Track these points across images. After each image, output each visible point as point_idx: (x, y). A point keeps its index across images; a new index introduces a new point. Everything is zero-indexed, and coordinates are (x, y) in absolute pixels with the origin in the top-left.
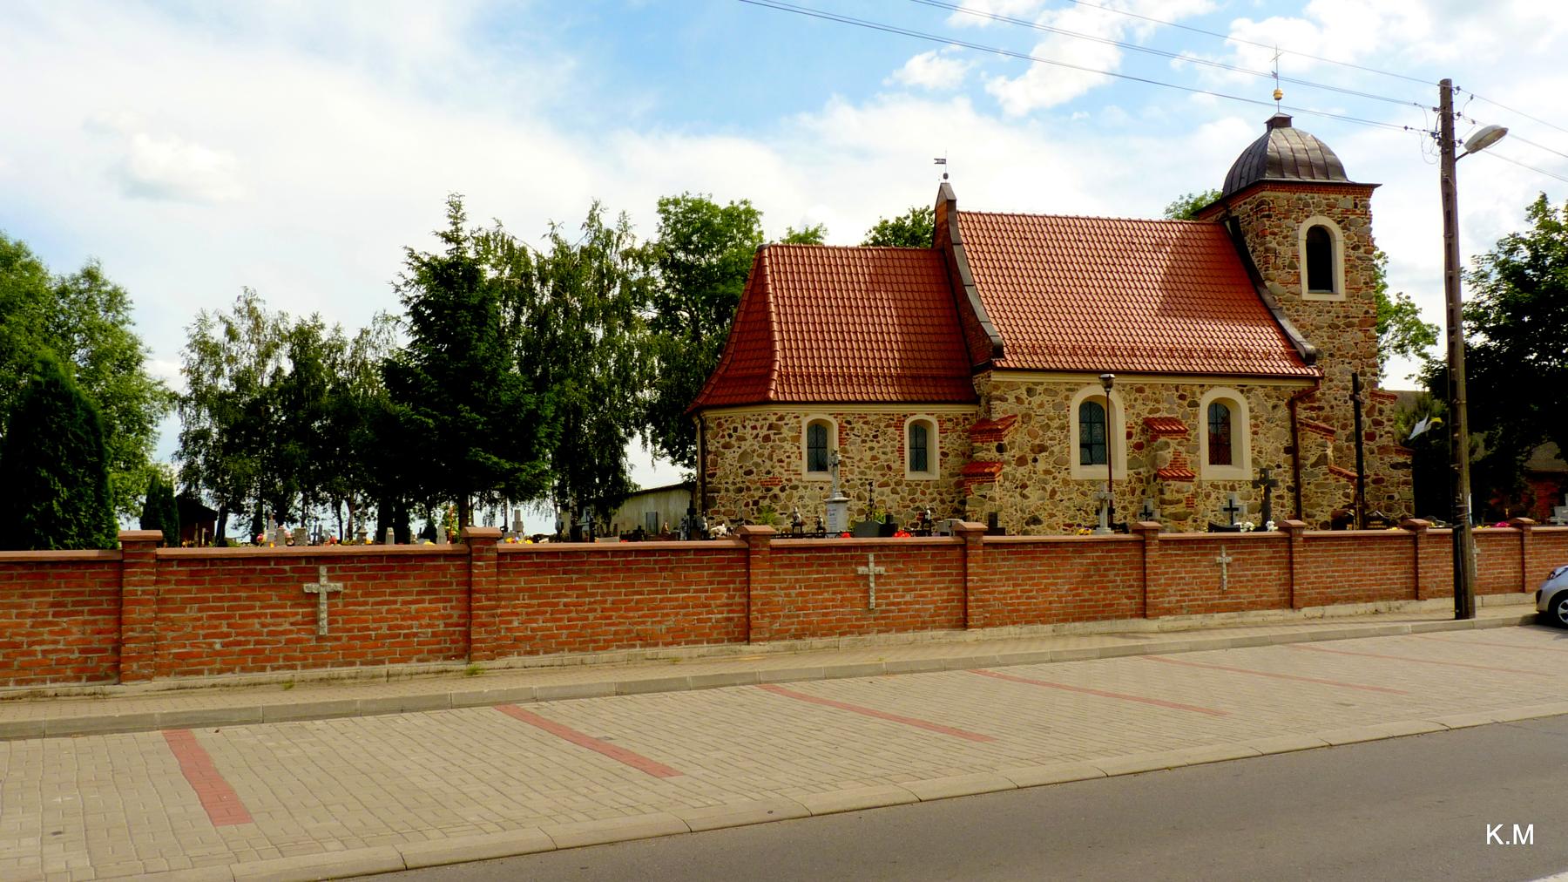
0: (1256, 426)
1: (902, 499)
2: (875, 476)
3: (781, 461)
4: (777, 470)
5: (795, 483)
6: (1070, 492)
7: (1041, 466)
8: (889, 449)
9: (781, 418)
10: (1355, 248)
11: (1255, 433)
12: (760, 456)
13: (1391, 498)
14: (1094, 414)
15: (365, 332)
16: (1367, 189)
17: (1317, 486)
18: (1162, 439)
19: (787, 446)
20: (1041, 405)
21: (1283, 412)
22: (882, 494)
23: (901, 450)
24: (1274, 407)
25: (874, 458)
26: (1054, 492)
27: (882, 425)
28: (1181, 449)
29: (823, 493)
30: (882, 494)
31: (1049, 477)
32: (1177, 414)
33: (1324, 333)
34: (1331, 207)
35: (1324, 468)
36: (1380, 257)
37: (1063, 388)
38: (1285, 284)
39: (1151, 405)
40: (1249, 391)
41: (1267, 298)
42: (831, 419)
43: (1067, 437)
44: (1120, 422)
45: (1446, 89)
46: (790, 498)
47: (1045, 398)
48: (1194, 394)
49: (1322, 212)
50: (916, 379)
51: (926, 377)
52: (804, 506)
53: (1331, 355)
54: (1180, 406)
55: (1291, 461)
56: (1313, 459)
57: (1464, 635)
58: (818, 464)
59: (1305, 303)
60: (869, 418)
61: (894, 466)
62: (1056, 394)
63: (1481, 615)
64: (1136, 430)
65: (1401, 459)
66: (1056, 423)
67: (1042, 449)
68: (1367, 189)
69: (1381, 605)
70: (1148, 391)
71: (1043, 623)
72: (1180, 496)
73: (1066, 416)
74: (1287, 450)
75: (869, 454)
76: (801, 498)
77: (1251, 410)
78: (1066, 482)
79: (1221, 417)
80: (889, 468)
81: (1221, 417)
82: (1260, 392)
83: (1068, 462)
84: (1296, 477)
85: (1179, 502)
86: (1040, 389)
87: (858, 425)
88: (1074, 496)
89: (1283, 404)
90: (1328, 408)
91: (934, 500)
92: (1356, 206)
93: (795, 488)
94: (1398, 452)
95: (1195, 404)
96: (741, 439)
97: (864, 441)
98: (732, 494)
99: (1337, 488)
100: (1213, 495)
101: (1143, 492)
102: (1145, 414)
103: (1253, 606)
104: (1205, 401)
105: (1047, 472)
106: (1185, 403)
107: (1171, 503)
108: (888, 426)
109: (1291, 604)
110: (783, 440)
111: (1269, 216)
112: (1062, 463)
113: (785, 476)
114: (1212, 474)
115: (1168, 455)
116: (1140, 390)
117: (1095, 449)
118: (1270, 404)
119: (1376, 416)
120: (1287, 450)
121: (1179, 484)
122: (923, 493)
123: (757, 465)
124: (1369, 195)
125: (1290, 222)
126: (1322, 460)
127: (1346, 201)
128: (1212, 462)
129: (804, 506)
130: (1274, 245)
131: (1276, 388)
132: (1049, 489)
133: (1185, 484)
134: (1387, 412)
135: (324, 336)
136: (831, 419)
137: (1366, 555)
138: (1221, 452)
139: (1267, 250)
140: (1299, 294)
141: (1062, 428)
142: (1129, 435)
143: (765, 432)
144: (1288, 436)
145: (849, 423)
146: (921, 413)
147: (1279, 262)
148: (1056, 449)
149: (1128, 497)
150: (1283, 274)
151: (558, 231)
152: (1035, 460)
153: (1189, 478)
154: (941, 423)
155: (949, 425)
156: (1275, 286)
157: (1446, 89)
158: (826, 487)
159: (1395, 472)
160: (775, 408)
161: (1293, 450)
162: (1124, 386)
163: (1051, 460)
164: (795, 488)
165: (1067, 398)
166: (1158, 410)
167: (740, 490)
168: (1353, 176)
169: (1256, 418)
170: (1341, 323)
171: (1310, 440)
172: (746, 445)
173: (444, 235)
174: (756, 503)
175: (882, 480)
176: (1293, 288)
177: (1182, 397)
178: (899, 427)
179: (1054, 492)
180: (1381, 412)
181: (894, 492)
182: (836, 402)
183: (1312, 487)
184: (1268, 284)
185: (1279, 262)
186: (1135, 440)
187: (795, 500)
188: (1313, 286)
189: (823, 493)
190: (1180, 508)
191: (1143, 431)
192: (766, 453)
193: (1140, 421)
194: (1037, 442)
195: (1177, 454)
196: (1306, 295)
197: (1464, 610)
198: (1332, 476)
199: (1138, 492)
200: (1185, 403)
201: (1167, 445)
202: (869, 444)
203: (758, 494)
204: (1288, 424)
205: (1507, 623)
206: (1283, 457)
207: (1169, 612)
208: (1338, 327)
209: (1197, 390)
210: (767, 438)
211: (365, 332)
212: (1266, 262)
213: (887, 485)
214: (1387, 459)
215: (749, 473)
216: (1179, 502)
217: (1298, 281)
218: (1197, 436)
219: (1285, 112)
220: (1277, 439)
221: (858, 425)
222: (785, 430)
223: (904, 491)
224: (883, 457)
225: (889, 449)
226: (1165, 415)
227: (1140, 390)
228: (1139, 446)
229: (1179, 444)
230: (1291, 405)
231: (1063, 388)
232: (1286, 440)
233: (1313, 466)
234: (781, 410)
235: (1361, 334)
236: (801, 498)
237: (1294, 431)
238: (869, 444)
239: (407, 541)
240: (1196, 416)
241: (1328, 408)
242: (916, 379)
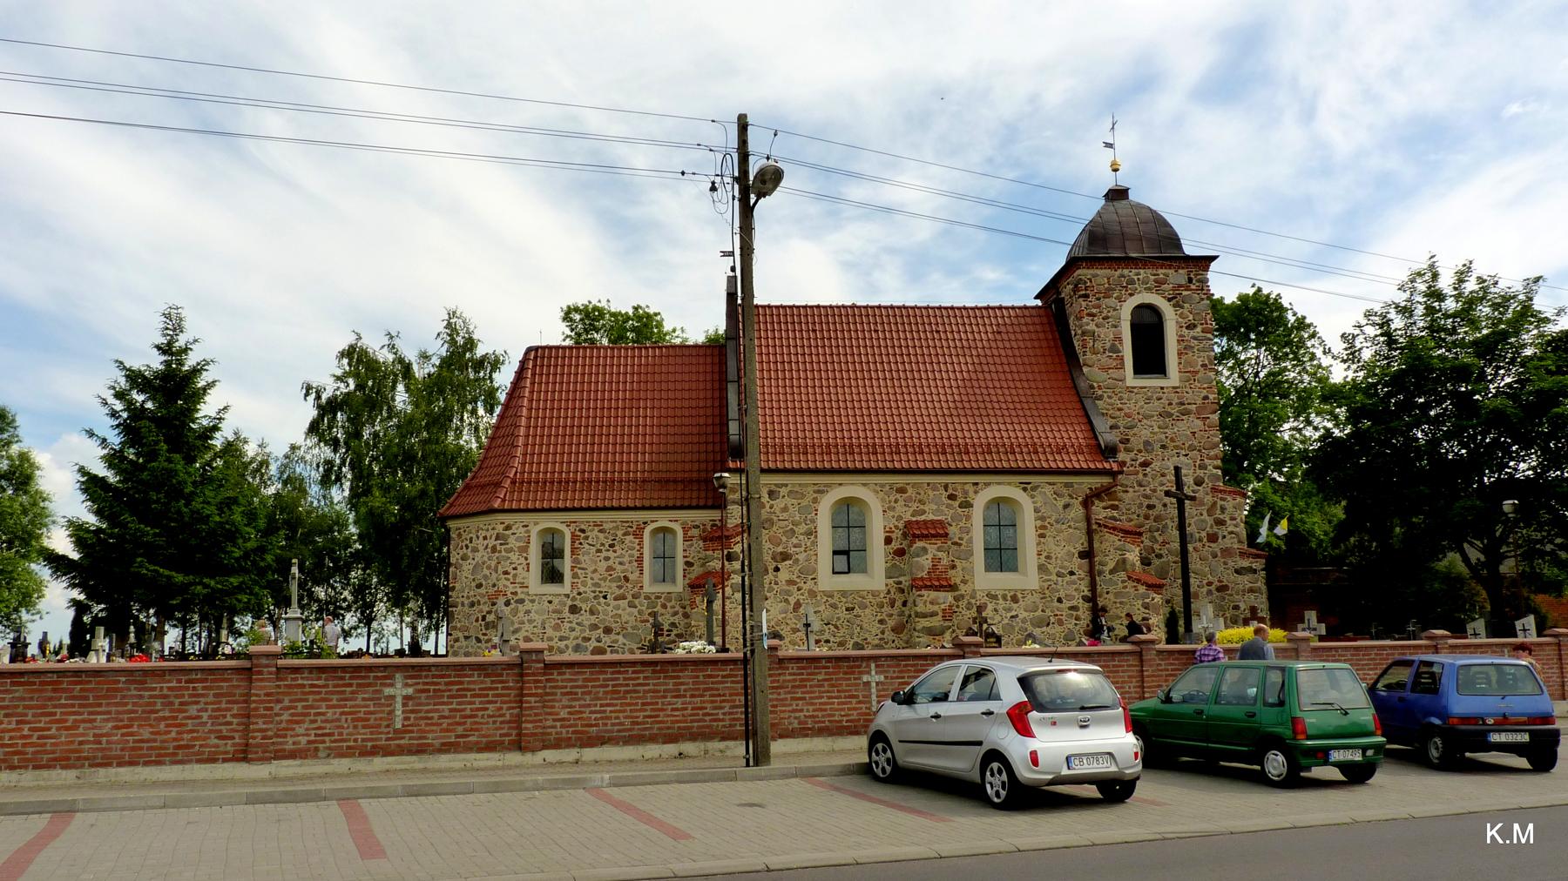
0: (1043, 527)
1: (640, 612)
2: (611, 588)
3: (506, 573)
4: (500, 584)
5: (521, 596)
6: (817, 604)
7: (784, 575)
8: (626, 559)
9: (508, 528)
10: (1191, 327)
11: (1042, 536)
12: (489, 568)
13: (1236, 608)
14: (849, 517)
15: (293, 448)
16: (1205, 262)
17: (1117, 595)
18: (919, 544)
19: (514, 557)
20: (785, 509)
21: (1077, 511)
22: (618, 608)
23: (640, 560)
24: (1066, 506)
25: (610, 569)
26: (798, 605)
27: (620, 533)
28: (940, 554)
29: (551, 607)
30: (618, 608)
31: (793, 588)
32: (946, 515)
33: (1155, 423)
34: (1159, 283)
35: (1123, 575)
36: (1313, 336)
37: (810, 489)
38: (1105, 369)
39: (914, 506)
40: (1033, 489)
41: (1082, 385)
42: (562, 527)
43: (814, 543)
44: (877, 526)
45: (743, 125)
46: (515, 612)
47: (789, 501)
48: (966, 493)
49: (1149, 289)
50: (664, 483)
51: (675, 481)
52: (530, 621)
53: (1163, 447)
54: (948, 506)
55: (1086, 568)
56: (1111, 565)
57: (751, 788)
58: (552, 575)
59: (1130, 390)
60: (606, 526)
61: (631, 577)
62: (803, 496)
63: (775, 765)
64: (897, 534)
65: (1245, 563)
66: (803, 528)
67: (785, 557)
68: (1205, 262)
69: (689, 747)
70: (910, 490)
71: (64, 767)
72: (936, 608)
73: (813, 521)
74: (1082, 555)
75: (604, 565)
76: (528, 612)
77: (1036, 510)
78: (812, 594)
79: (1002, 519)
80: (626, 579)
81: (1002, 519)
82: (1048, 490)
83: (815, 571)
84: (1093, 586)
85: (933, 614)
86: (783, 491)
87: (593, 534)
88: (822, 608)
89: (1077, 503)
90: (1159, 507)
91: (676, 614)
92: (1190, 280)
93: (521, 601)
94: (1243, 554)
95: (967, 505)
96: (475, 550)
97: (599, 551)
98: (466, 609)
99: (1137, 597)
100: (990, 607)
101: (904, 604)
102: (907, 517)
103: (446, 748)
104: (980, 500)
105: (790, 582)
106: (957, 504)
107: (924, 616)
108: (625, 534)
109: (519, 746)
110: (510, 550)
111: (1086, 296)
112: (809, 572)
113: (511, 588)
114: (984, 580)
115: (925, 562)
116: (902, 491)
117: (848, 556)
118: (1061, 503)
119: (1218, 514)
120: (1082, 555)
121: (933, 594)
122: (664, 606)
123: (486, 577)
124: (1207, 269)
125: (1112, 302)
126: (1122, 564)
127: (1178, 276)
128: (988, 568)
129: (530, 621)
130: (1092, 327)
131: (1067, 485)
132: (792, 600)
133: (941, 594)
134: (1230, 509)
135: (251, 450)
136: (562, 527)
137: (20, 691)
138: (1002, 557)
139: (1084, 333)
140: (1123, 380)
141: (809, 533)
142: (888, 541)
143: (492, 542)
144: (1084, 539)
145: (583, 531)
146: (663, 519)
147: (1099, 345)
148: (801, 557)
149: (887, 609)
150: (1104, 359)
151: (397, 342)
152: (777, 569)
153: (952, 588)
154: (685, 530)
155: (695, 532)
156: (1094, 371)
157: (743, 125)
158: (556, 601)
159: (1240, 578)
160: (501, 517)
161: (1088, 554)
162: (882, 486)
163: (796, 569)
164: (521, 601)
165: (815, 501)
166: (924, 512)
167: (472, 605)
168: (1190, 249)
169: (1043, 519)
170: (1174, 410)
171: (1109, 545)
172: (478, 556)
173: (158, 347)
174: (484, 618)
175: (618, 592)
176: (1115, 374)
177: (952, 497)
178: (638, 534)
179: (798, 605)
180: (1223, 509)
181: (632, 605)
182: (566, 509)
183: (1111, 596)
184: (1085, 369)
185: (1099, 345)
186: (895, 545)
187: (521, 614)
188: (1139, 370)
189: (551, 607)
190: (936, 622)
191: (905, 535)
192: (493, 564)
193: (901, 525)
194: (780, 549)
195: (936, 560)
196: (1131, 380)
197: (759, 757)
198: (1130, 584)
199: (898, 604)
200: (957, 504)
201: (925, 550)
202: (604, 554)
203: (486, 608)
204: (1083, 525)
205: (808, 774)
206: (1078, 564)
207: (292, 755)
208: (1170, 415)
209: (971, 489)
210: (494, 549)
211: (293, 448)
212: (1084, 347)
213: (624, 598)
214: (1231, 564)
215: (479, 586)
216: (933, 614)
217: (1122, 367)
218: (970, 541)
219: (1123, 183)
220: (1069, 541)
221: (593, 534)
222: (512, 540)
223: (642, 604)
224: (619, 568)
225: (626, 559)
226: (931, 517)
227: (902, 491)
228: (900, 553)
229: (939, 550)
230: (1087, 503)
231: (810, 489)
232: (1080, 544)
233: (1111, 572)
234: (509, 518)
235: (1199, 423)
236: (528, 612)
237: (1090, 533)
238: (604, 554)
239: (24, 659)
240: (968, 518)
241: (1159, 507)
242: (664, 483)
